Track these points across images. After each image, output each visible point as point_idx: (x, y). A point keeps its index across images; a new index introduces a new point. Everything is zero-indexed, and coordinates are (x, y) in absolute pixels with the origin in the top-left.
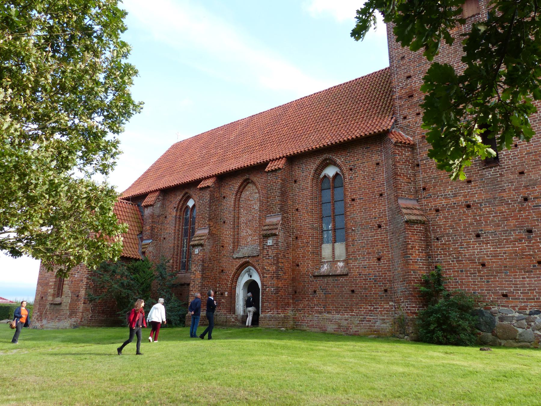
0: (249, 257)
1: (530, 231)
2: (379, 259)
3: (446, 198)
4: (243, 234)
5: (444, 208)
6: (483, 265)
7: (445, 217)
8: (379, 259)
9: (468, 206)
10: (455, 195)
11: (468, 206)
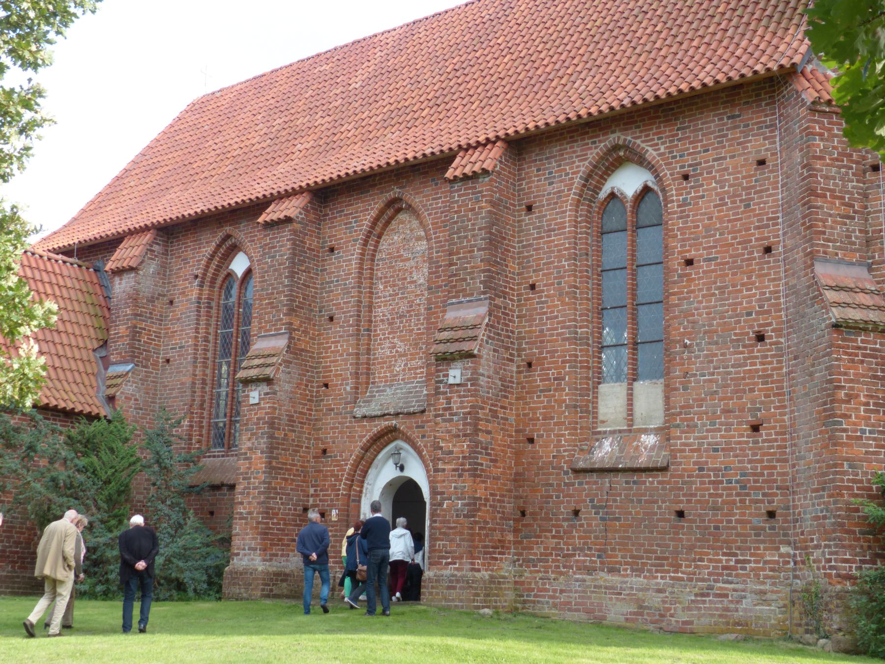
2: (755, 428)
4: (382, 351)
8: (755, 428)
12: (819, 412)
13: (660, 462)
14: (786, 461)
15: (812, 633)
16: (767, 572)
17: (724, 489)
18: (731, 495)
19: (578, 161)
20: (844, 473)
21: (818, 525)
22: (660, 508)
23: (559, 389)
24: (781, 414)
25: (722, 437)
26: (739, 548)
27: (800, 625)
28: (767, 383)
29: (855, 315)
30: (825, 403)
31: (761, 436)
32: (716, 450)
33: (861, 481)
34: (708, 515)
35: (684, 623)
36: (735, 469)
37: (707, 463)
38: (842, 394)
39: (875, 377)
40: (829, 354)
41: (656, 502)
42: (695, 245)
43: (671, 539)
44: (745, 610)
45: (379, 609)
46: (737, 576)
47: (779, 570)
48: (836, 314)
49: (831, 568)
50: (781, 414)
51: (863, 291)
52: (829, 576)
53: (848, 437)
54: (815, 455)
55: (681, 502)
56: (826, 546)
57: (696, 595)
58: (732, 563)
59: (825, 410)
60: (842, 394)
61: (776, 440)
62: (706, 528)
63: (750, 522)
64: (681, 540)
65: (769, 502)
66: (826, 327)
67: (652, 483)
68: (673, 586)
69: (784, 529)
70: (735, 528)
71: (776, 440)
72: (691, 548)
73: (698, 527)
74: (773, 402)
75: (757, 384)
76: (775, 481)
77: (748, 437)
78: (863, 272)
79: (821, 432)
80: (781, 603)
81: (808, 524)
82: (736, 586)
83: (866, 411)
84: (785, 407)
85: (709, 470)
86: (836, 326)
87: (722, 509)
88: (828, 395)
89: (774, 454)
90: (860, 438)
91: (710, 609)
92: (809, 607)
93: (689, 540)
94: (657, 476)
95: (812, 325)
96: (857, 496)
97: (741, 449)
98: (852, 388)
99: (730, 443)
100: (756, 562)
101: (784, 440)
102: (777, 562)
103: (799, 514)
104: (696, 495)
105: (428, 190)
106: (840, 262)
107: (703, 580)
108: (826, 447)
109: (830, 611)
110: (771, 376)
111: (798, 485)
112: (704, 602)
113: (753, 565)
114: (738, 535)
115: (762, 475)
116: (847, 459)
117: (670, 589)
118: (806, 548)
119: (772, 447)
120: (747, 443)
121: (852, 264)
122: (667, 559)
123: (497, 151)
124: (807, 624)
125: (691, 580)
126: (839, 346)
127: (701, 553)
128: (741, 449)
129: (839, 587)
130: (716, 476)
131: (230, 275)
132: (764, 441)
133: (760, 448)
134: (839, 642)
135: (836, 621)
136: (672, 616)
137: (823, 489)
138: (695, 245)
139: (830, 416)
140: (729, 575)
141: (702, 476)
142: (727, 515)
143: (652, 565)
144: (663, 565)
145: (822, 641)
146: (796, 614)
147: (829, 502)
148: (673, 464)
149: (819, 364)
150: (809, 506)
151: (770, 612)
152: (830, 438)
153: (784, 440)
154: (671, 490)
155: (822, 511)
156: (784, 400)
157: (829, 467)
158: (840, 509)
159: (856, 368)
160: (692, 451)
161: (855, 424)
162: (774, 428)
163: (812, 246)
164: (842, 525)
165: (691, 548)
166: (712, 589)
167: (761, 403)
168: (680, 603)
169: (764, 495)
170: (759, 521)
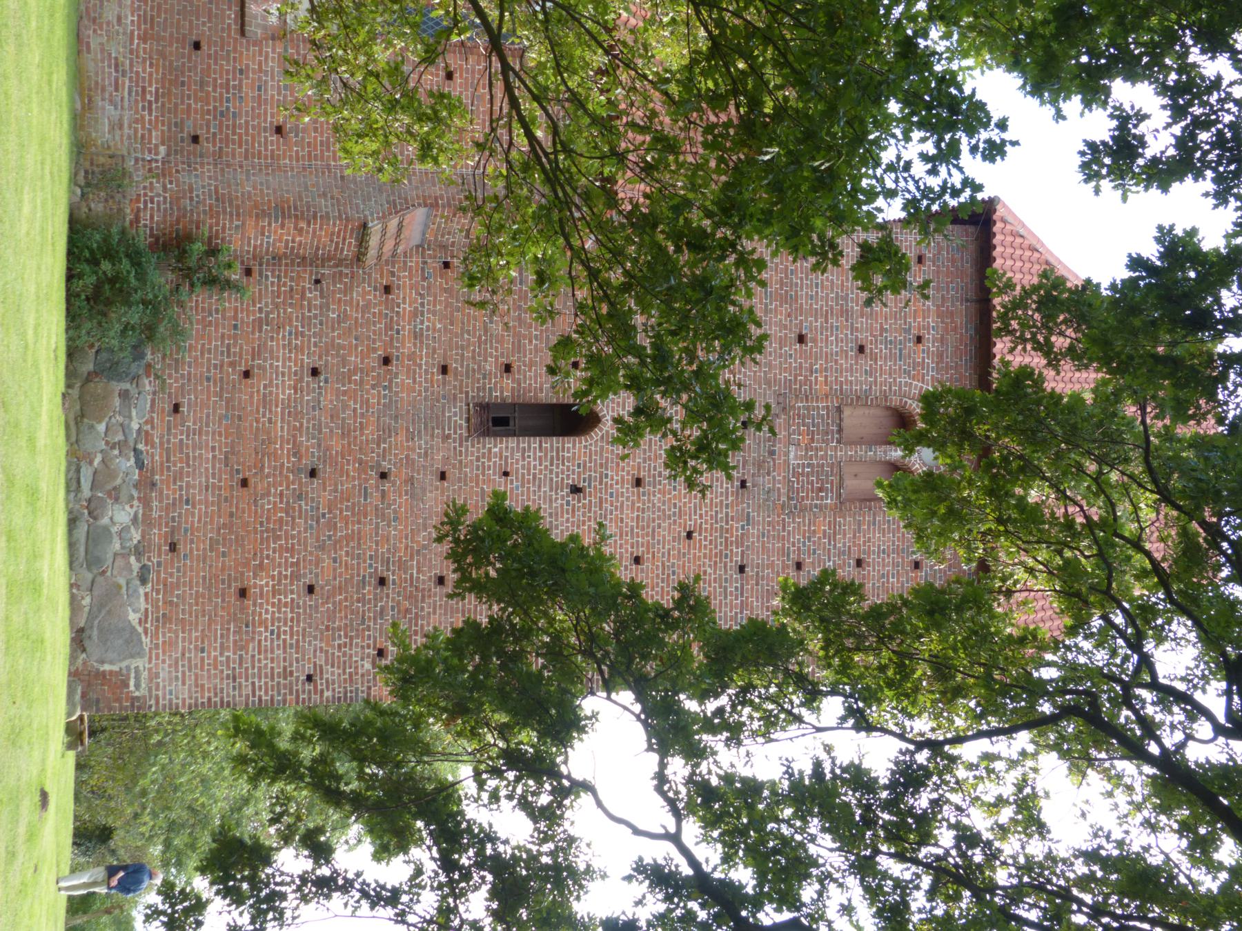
2: (279, 130)
8: (279, 130)
12: (288, 199)
13: (253, 29)
14: (246, 158)
15: (86, 178)
16: (140, 132)
17: (221, 94)
18: (215, 101)
20: (231, 221)
21: (184, 190)
22: (204, 23)
24: (291, 156)
25: (273, 96)
26: (163, 105)
27: (92, 164)
28: (322, 145)
29: (374, 241)
30: (296, 209)
31: (271, 135)
32: (259, 90)
33: (224, 231)
34: (196, 75)
35: (88, 44)
36: (241, 107)
37: (247, 78)
38: (303, 225)
39: (318, 249)
40: (340, 217)
41: (210, 21)
42: (466, 84)
43: (171, 35)
44: (103, 108)
46: (136, 101)
47: (142, 143)
48: (375, 227)
49: (145, 202)
50: (291, 156)
51: (397, 244)
52: (138, 201)
53: (263, 227)
54: (249, 192)
55: (209, 49)
56: (165, 198)
57: (116, 58)
58: (148, 97)
59: (289, 208)
60: (303, 225)
61: (266, 150)
62: (183, 73)
63: (188, 118)
64: (171, 45)
65: (207, 139)
66: (365, 216)
67: (229, 18)
68: (124, 34)
69: (182, 151)
70: (183, 103)
71: (266, 150)
72: (162, 54)
73: (183, 64)
74: (303, 150)
75: (322, 136)
76: (227, 146)
77: (271, 123)
78: (416, 239)
79: (269, 201)
80: (112, 144)
81: (185, 178)
82: (126, 99)
83: (287, 241)
84: (298, 160)
85: (241, 80)
86: (365, 226)
87: (202, 91)
88: (302, 212)
89: (253, 147)
90: (263, 234)
91: (103, 72)
92: (109, 176)
93: (171, 53)
94: (236, 24)
95: (370, 200)
96: (211, 227)
97: (259, 114)
98: (308, 232)
99: (266, 104)
100: (150, 121)
101: (266, 158)
102: (150, 142)
103: (196, 169)
104: (216, 64)
106: (426, 226)
107: (131, 65)
108: (256, 207)
109: (106, 201)
110: (328, 150)
111: (222, 170)
112: (110, 67)
113: (147, 118)
114: (176, 104)
115: (234, 134)
116: (243, 224)
117: (121, 30)
118: (164, 175)
119: (260, 146)
120: (265, 121)
121: (424, 234)
122: (152, 28)
124: (93, 173)
125: (131, 52)
126: (346, 226)
127: (157, 65)
128: (259, 114)
129: (128, 211)
130: (234, 87)
132: (266, 138)
133: (259, 134)
134: (79, 208)
135: (98, 207)
136: (95, 31)
137: (217, 199)
138: (466, 84)
139: (283, 213)
140: (137, 94)
141: (234, 73)
142: (196, 95)
143: (145, 11)
144: (145, 23)
145: (79, 191)
146: (102, 160)
147: (205, 205)
148: (248, 42)
149: (333, 205)
150: (201, 181)
151: (102, 133)
152: (263, 211)
153: (266, 158)
154: (222, 37)
155: (197, 196)
156: (303, 160)
157: (238, 207)
158: (198, 214)
159: (326, 236)
160: (260, 63)
161: (276, 232)
162: (278, 149)
163: (443, 206)
164: (185, 216)
165: (162, 54)
166: (123, 76)
167: (303, 138)
168: (108, 40)
169: (214, 134)
170: (189, 128)
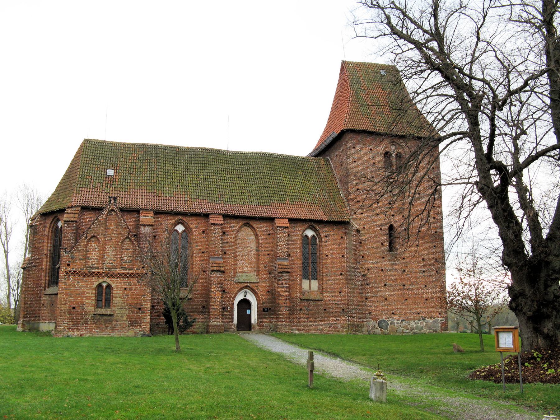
0: (249, 283)
1: (404, 285)
2: (340, 293)
3: (373, 264)
4: (240, 264)
5: (371, 269)
6: (386, 299)
7: (372, 274)
8: (340, 293)
9: (382, 270)
10: (377, 264)
11: (382, 270)
19: (172, 220)
23: (296, 280)
45: (170, 332)
105: (258, 223)
123: (79, 209)
131: (57, 227)
